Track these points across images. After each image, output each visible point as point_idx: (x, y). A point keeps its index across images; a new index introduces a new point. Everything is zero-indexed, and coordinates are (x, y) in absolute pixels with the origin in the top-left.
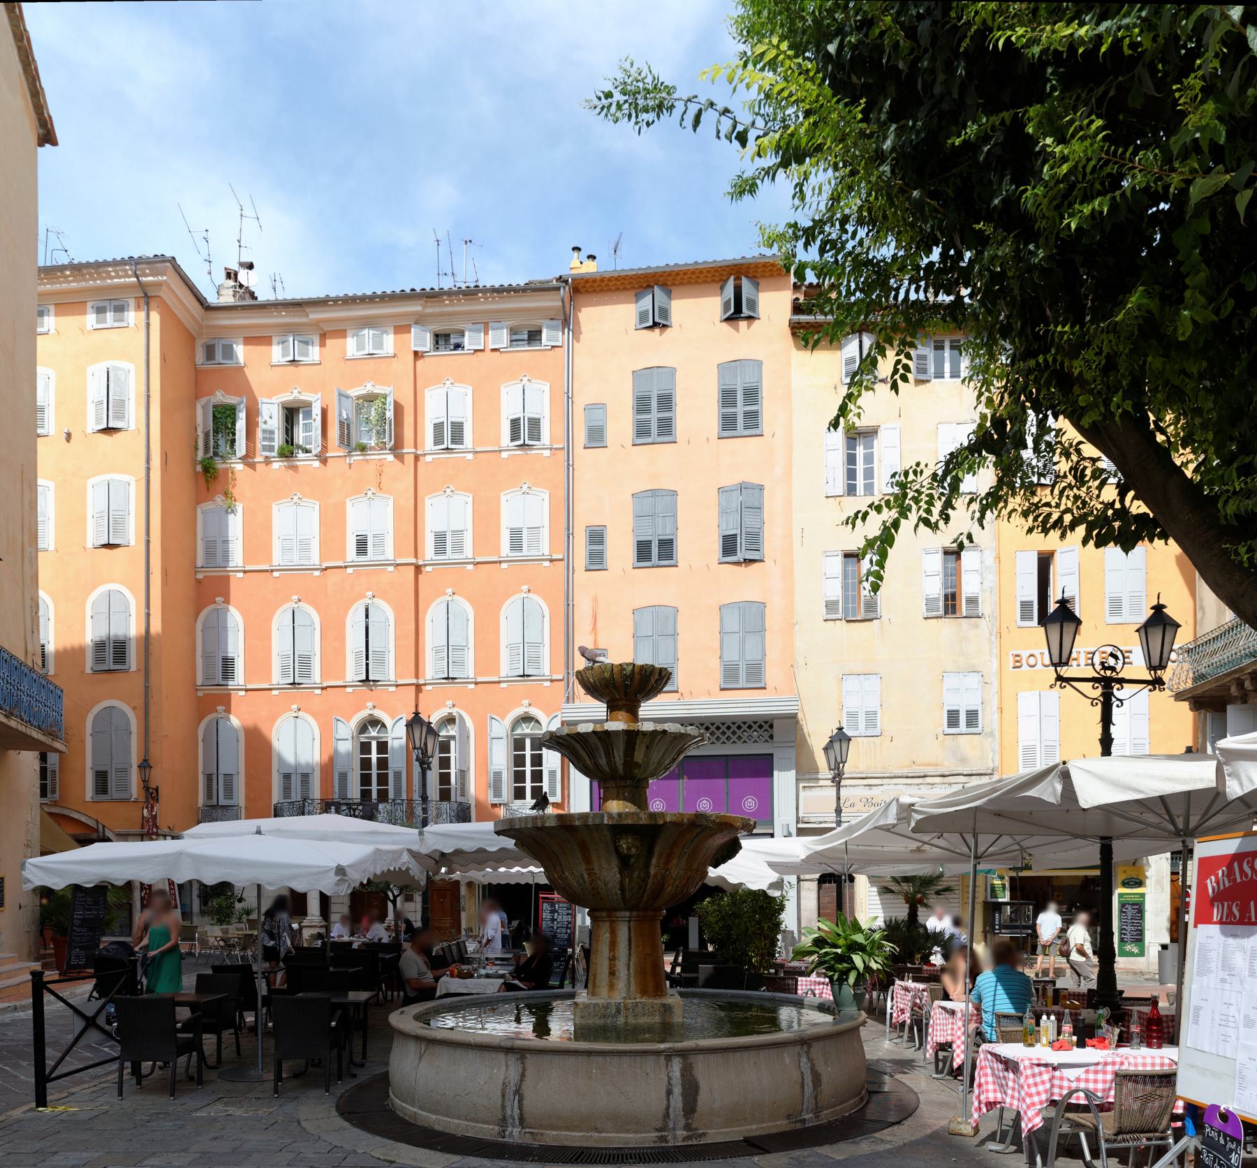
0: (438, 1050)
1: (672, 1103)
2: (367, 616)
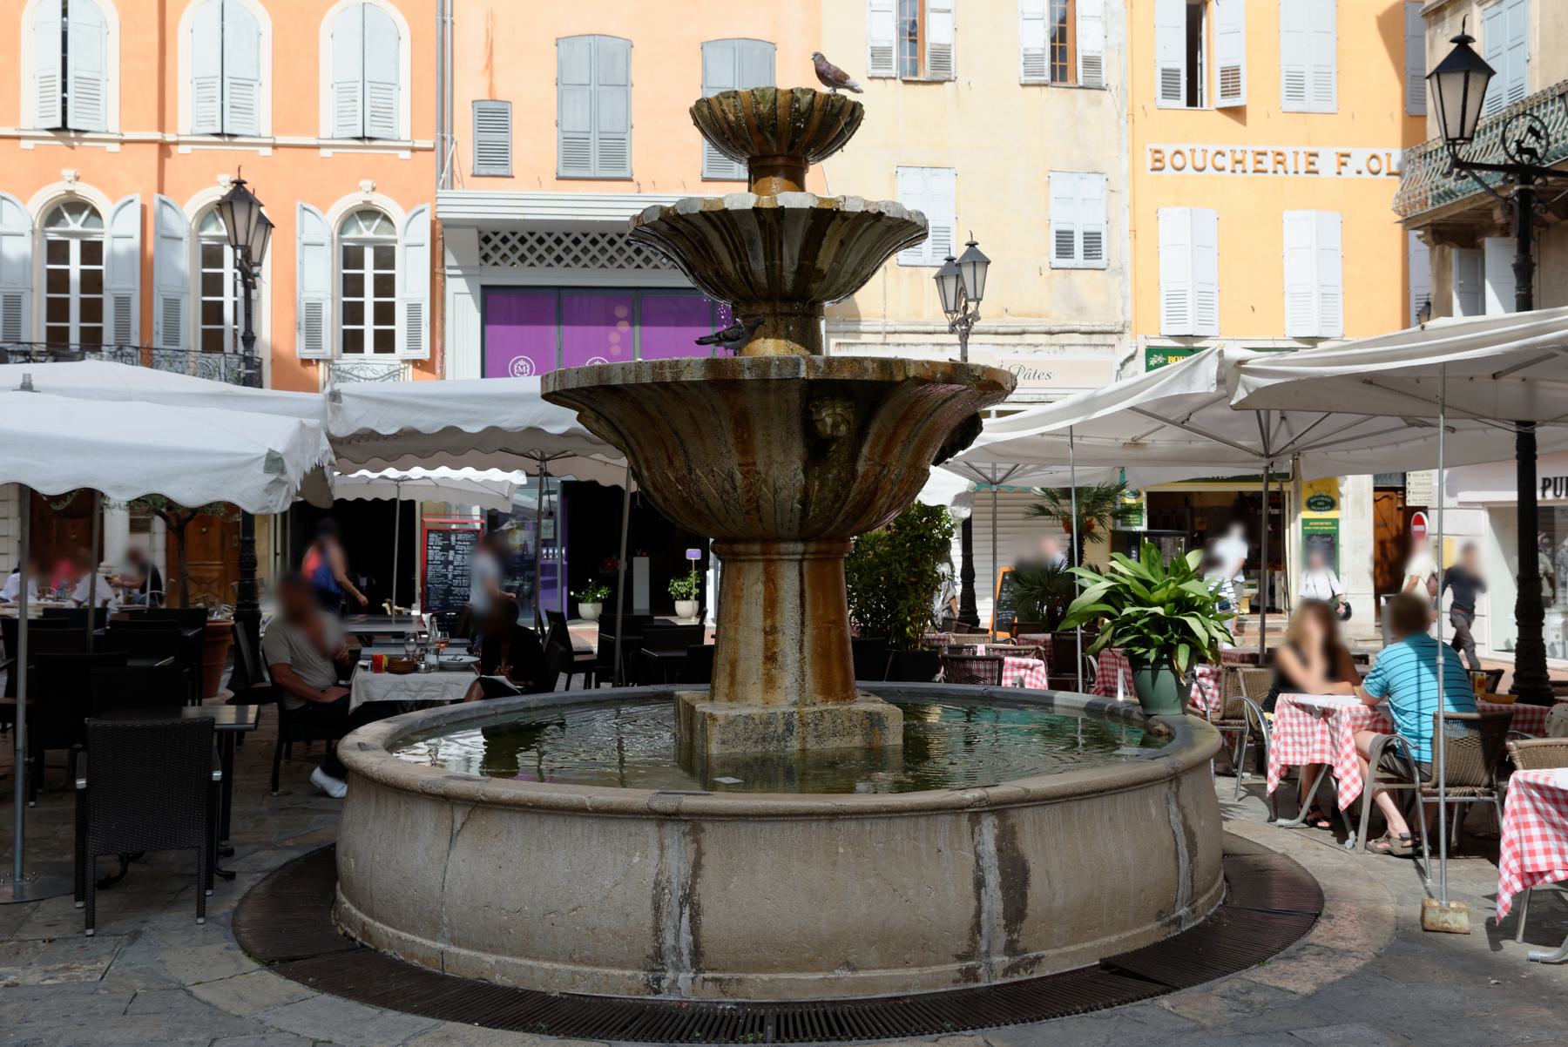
0: (498, 821)
1: (986, 904)
2: (65, 13)
